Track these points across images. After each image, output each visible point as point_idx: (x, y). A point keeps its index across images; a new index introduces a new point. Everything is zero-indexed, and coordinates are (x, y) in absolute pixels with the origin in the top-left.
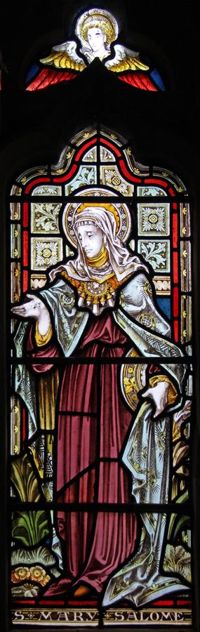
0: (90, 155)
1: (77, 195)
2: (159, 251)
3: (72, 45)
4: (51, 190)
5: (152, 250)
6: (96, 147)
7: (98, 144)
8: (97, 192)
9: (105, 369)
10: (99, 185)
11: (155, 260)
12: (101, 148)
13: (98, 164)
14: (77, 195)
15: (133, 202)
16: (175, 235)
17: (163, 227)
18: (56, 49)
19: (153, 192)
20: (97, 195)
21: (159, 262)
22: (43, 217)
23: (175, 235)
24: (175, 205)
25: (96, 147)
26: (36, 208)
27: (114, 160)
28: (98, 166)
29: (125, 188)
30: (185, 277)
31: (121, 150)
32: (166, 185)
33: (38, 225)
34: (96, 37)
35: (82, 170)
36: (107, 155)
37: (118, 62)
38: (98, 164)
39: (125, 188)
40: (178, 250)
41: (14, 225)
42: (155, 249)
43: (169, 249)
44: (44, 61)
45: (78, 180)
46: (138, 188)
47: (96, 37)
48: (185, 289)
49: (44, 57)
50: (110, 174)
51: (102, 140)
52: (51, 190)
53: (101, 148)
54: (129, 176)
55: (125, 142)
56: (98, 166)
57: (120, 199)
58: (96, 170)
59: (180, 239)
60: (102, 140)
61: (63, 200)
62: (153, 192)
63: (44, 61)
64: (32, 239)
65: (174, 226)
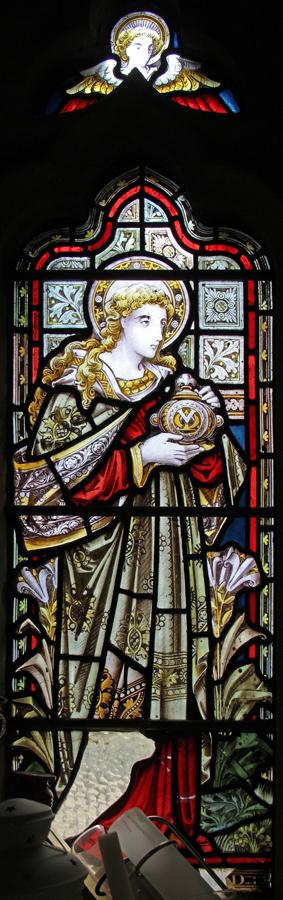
0: (130, 214)
1: (110, 267)
2: (229, 351)
3: (111, 64)
4: (79, 263)
5: (219, 351)
6: (138, 201)
7: (141, 196)
8: (138, 263)
9: (72, 560)
10: (142, 252)
11: (224, 366)
12: (146, 201)
13: (142, 225)
14: (110, 267)
15: (193, 276)
16: (252, 382)
17: (236, 318)
18: (85, 73)
19: (220, 263)
20: (136, 267)
21: (229, 369)
22: (62, 302)
23: (252, 382)
24: (251, 284)
25: (138, 201)
26: (53, 289)
27: (166, 220)
28: (149, 229)
29: (184, 259)
30: (264, 362)
31: (172, 200)
32: (236, 251)
33: (52, 315)
34: (139, 44)
35: (120, 236)
36: (155, 213)
37: (173, 78)
38: (142, 225)
39: (184, 259)
40: (256, 403)
41: (269, 451)
42: (224, 349)
43: (242, 349)
44: (72, 92)
45: (112, 250)
46: (241, 392)
47: (139, 44)
48: (264, 377)
49: (71, 86)
50: (162, 241)
51: (147, 190)
52: (79, 263)
53: (146, 201)
54: (181, 238)
55: (177, 188)
56: (149, 229)
57: (175, 273)
58: (138, 237)
59: (259, 385)
60: (147, 190)
61: (90, 275)
62: (220, 263)
63: (72, 92)
64: (45, 336)
65: (251, 308)
